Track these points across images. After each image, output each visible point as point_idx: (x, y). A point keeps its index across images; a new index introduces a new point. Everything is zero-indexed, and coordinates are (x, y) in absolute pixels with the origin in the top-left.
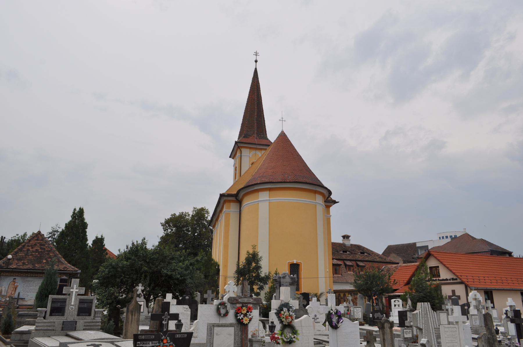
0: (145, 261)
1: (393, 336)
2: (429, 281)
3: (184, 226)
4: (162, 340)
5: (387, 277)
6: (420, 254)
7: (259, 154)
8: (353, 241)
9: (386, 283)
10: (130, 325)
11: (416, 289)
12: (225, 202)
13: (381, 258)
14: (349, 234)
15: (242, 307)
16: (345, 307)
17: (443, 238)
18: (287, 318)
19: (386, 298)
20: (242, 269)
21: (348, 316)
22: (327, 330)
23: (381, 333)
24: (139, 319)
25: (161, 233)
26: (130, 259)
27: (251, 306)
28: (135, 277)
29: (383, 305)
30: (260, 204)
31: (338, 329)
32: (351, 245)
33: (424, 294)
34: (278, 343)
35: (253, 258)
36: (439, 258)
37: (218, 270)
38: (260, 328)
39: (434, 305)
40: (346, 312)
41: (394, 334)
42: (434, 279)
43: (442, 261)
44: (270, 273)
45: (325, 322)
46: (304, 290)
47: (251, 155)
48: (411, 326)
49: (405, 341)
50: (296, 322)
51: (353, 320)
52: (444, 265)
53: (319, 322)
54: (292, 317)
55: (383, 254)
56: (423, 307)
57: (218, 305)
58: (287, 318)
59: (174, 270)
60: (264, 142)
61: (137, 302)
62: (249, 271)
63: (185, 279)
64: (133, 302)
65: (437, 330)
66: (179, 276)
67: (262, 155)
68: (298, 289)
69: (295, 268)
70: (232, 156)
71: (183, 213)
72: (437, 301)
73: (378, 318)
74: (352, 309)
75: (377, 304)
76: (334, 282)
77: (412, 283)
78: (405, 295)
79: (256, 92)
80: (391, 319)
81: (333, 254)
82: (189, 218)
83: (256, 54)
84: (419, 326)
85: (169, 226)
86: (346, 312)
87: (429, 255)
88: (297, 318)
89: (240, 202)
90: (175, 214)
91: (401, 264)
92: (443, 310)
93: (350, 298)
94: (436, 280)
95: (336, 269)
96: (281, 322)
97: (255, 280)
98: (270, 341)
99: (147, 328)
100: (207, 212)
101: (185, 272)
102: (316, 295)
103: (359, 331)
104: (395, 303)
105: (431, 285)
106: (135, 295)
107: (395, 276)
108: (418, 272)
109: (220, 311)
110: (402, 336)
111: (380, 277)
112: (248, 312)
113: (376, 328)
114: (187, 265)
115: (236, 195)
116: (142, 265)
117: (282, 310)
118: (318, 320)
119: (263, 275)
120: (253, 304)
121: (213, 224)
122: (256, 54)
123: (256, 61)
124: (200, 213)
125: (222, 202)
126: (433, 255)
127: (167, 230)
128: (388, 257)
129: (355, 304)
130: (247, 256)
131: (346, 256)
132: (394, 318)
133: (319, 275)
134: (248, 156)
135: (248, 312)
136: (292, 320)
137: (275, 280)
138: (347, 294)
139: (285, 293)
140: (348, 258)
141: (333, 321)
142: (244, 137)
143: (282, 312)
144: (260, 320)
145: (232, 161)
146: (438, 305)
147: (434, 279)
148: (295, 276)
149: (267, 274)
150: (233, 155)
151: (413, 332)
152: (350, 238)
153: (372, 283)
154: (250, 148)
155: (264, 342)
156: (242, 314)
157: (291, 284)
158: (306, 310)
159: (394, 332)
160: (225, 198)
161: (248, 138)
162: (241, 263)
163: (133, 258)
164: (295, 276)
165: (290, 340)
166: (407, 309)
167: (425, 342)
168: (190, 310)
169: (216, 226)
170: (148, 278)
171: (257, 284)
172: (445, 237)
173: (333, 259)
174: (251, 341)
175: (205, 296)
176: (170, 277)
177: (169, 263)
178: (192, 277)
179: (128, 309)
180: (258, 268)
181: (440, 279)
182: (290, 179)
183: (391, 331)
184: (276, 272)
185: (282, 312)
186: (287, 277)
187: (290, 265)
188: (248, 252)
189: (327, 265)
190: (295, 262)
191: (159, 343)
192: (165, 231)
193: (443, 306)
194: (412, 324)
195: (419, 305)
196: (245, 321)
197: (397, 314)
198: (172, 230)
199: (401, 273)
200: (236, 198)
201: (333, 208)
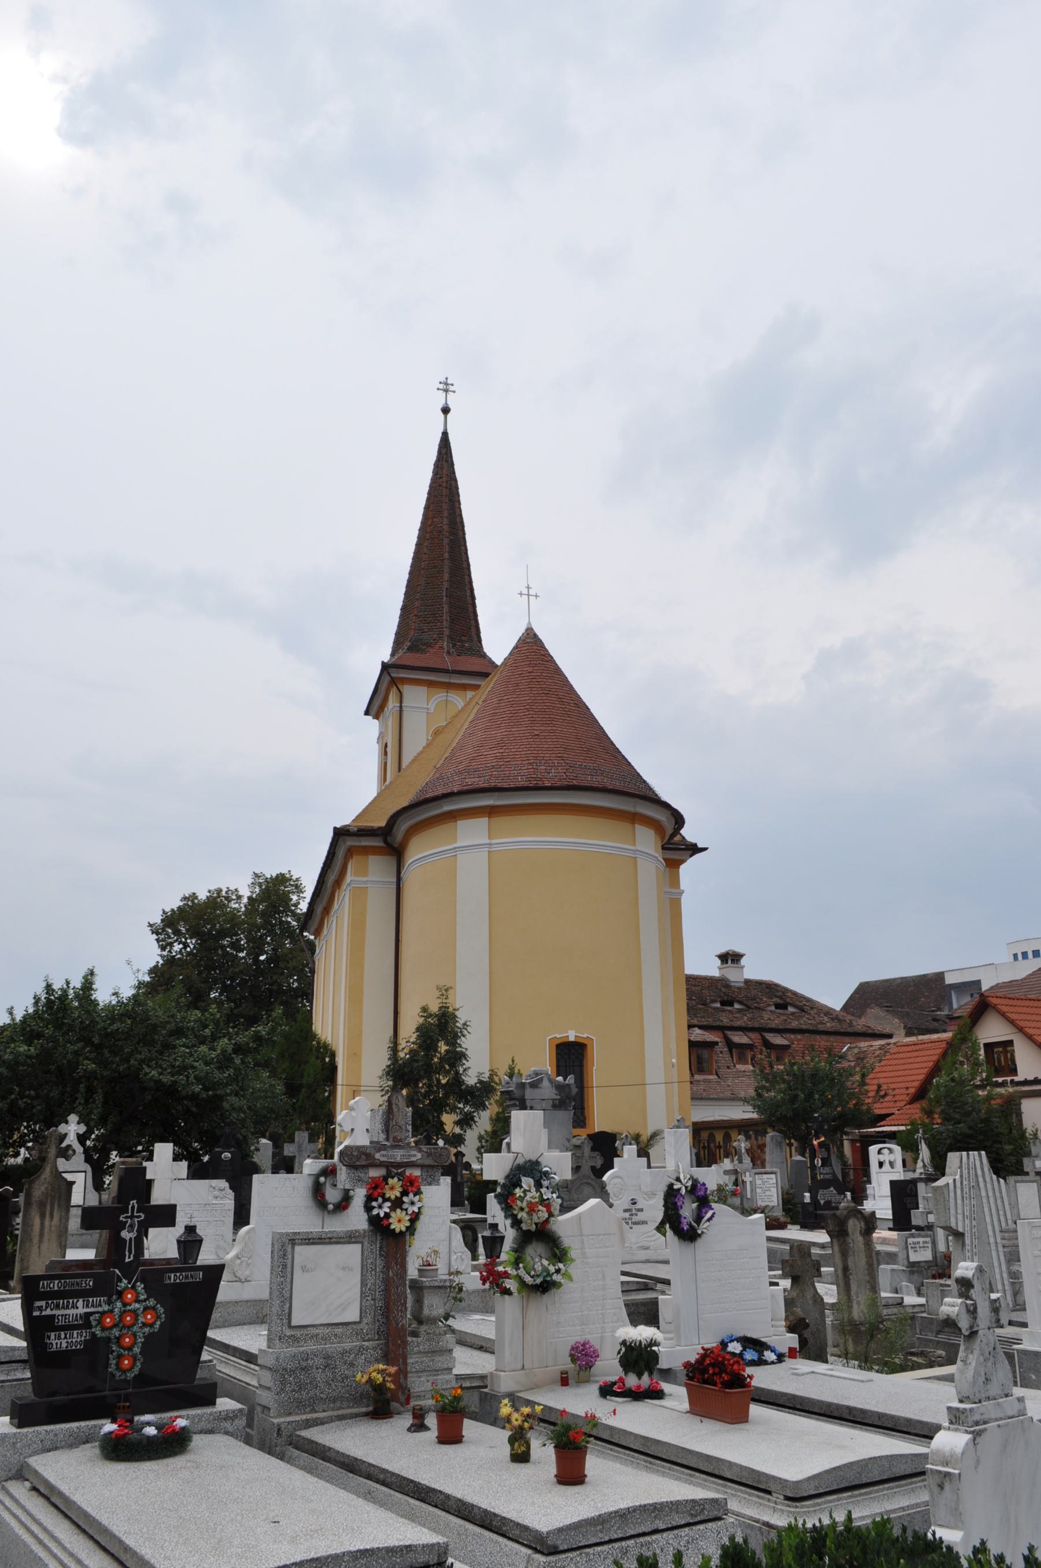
0: (88, 1042)
1: (874, 1259)
2: (982, 1087)
3: (222, 934)
4: (120, 1294)
5: (858, 1077)
6: (955, 1006)
7: (457, 700)
8: (753, 970)
9: (852, 1096)
10: (35, 1250)
11: (943, 1111)
12: (350, 852)
13: (840, 1021)
14: (738, 949)
15: (385, 1179)
16: (726, 1172)
17: (1025, 955)
18: (532, 1209)
19: (853, 1142)
20: (407, 1063)
21: (737, 1201)
22: (668, 1244)
23: (836, 1248)
24: (67, 1228)
25: (149, 955)
26: (39, 1035)
27: (417, 1172)
28: (55, 1093)
29: (844, 1163)
30: (462, 858)
31: (699, 1242)
32: (747, 982)
33: (970, 1128)
34: (507, 1292)
35: (442, 1027)
36: (1013, 1016)
37: (333, 1068)
38: (454, 1244)
39: (1001, 1161)
40: (731, 1187)
41: (878, 1253)
42: (1000, 1080)
43: (1022, 1024)
44: (493, 1073)
45: (662, 1224)
46: (600, 1121)
47: (432, 706)
48: (930, 1227)
49: (912, 1272)
50: (563, 1224)
51: (746, 1211)
52: (1030, 1037)
53: (644, 1223)
54: (548, 1207)
55: (845, 1008)
56: (966, 1166)
57: (317, 1176)
58: (532, 1209)
59: (183, 1068)
60: (471, 663)
61: (58, 1175)
62: (429, 1070)
63: (221, 1098)
64: (46, 1174)
65: (1010, 1235)
66: (197, 1089)
67: (467, 704)
68: (580, 1120)
69: (571, 1056)
70: (374, 710)
71: (219, 891)
72: (1008, 1148)
73: (828, 1203)
74: (748, 1178)
75: (826, 1162)
76: (696, 1098)
77: (931, 1095)
78: (910, 1133)
79: (445, 506)
80: (868, 1206)
81: (690, 1009)
82: (240, 907)
83: (446, 387)
84: (953, 1225)
85: (177, 932)
86: (731, 1187)
87: (984, 1007)
88: (565, 1209)
89: (397, 853)
90: (194, 896)
91: (900, 1038)
92: (1027, 1174)
93: (742, 1143)
94: (1003, 1084)
95: (699, 1057)
96: (516, 1223)
97: (446, 1096)
98: (478, 1285)
99: (89, 1254)
100: (297, 887)
101: (217, 1075)
102: (637, 1138)
103: (765, 1244)
104: (882, 1158)
105: (989, 1098)
106: (53, 1151)
107: (881, 1076)
108: (949, 1059)
109: (323, 1195)
110: (902, 1256)
111: (833, 1079)
112: (405, 1193)
113: (821, 1237)
114: (224, 1051)
115: (385, 833)
116: (76, 1053)
117: (518, 1184)
118: (641, 1216)
119: (470, 1080)
120: (422, 1166)
121: (314, 924)
122: (446, 387)
123: (446, 410)
124: (275, 892)
125: (341, 853)
126: (994, 1007)
127: (171, 945)
128: (860, 1017)
129: (758, 1160)
130: (421, 1020)
131: (731, 1016)
132: (879, 1202)
133: (647, 1080)
134: (423, 708)
135: (405, 1193)
136: (551, 1215)
137: (507, 1094)
138: (734, 1134)
139: (530, 1133)
140: (738, 1024)
141: (682, 1217)
142: (410, 649)
143: (518, 1192)
144: (454, 1222)
145: (373, 726)
146: (1013, 1159)
147: (1000, 1080)
148: (571, 1079)
149: (485, 1078)
150: (375, 708)
151: (934, 1243)
152: (743, 961)
153: (809, 1096)
154: (430, 684)
155: (461, 1290)
156: (385, 1200)
157: (558, 1105)
158: (603, 1186)
159: (879, 1247)
160: (351, 842)
161: (423, 651)
162: (402, 1044)
163: (48, 1032)
164: (571, 1079)
165: (545, 1281)
166: (916, 1175)
167: (969, 1274)
168: (231, 1194)
169: (325, 931)
170: (99, 1098)
171: (453, 1110)
172: (1030, 955)
173: (690, 1027)
174: (417, 1287)
175: (289, 1150)
176: (171, 1091)
177: (167, 1047)
178: (242, 1089)
179: (28, 1196)
180: (456, 1057)
181: (1016, 1079)
182: (554, 775)
183: (869, 1244)
184: (512, 1069)
185: (518, 1192)
186: (546, 1083)
187: (558, 1046)
188: (424, 1009)
189: (673, 1046)
190: (572, 1039)
191: (109, 1303)
192: (163, 948)
193: (1026, 1161)
194: (931, 1218)
195: (953, 1158)
196: (398, 1222)
197: (886, 1190)
198: (186, 945)
199: (898, 1063)
200: (385, 841)
201: (689, 869)
